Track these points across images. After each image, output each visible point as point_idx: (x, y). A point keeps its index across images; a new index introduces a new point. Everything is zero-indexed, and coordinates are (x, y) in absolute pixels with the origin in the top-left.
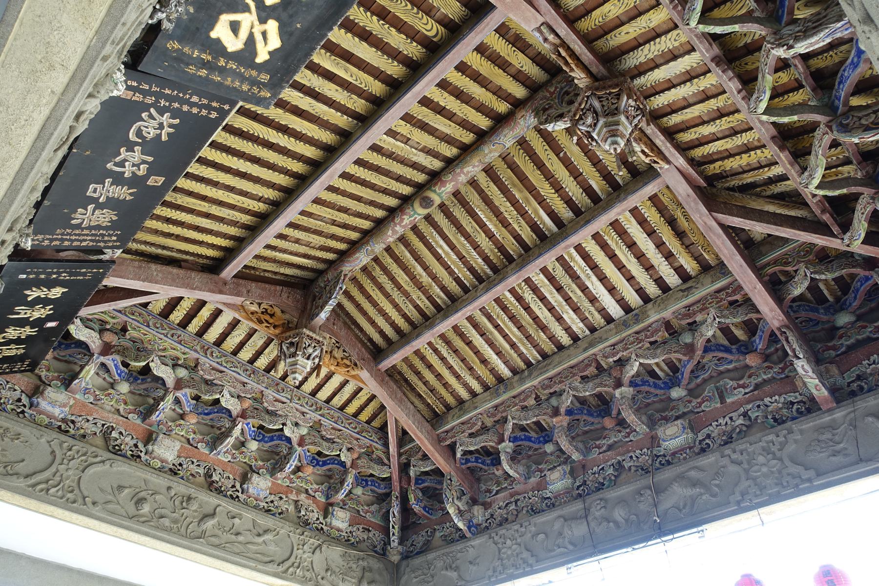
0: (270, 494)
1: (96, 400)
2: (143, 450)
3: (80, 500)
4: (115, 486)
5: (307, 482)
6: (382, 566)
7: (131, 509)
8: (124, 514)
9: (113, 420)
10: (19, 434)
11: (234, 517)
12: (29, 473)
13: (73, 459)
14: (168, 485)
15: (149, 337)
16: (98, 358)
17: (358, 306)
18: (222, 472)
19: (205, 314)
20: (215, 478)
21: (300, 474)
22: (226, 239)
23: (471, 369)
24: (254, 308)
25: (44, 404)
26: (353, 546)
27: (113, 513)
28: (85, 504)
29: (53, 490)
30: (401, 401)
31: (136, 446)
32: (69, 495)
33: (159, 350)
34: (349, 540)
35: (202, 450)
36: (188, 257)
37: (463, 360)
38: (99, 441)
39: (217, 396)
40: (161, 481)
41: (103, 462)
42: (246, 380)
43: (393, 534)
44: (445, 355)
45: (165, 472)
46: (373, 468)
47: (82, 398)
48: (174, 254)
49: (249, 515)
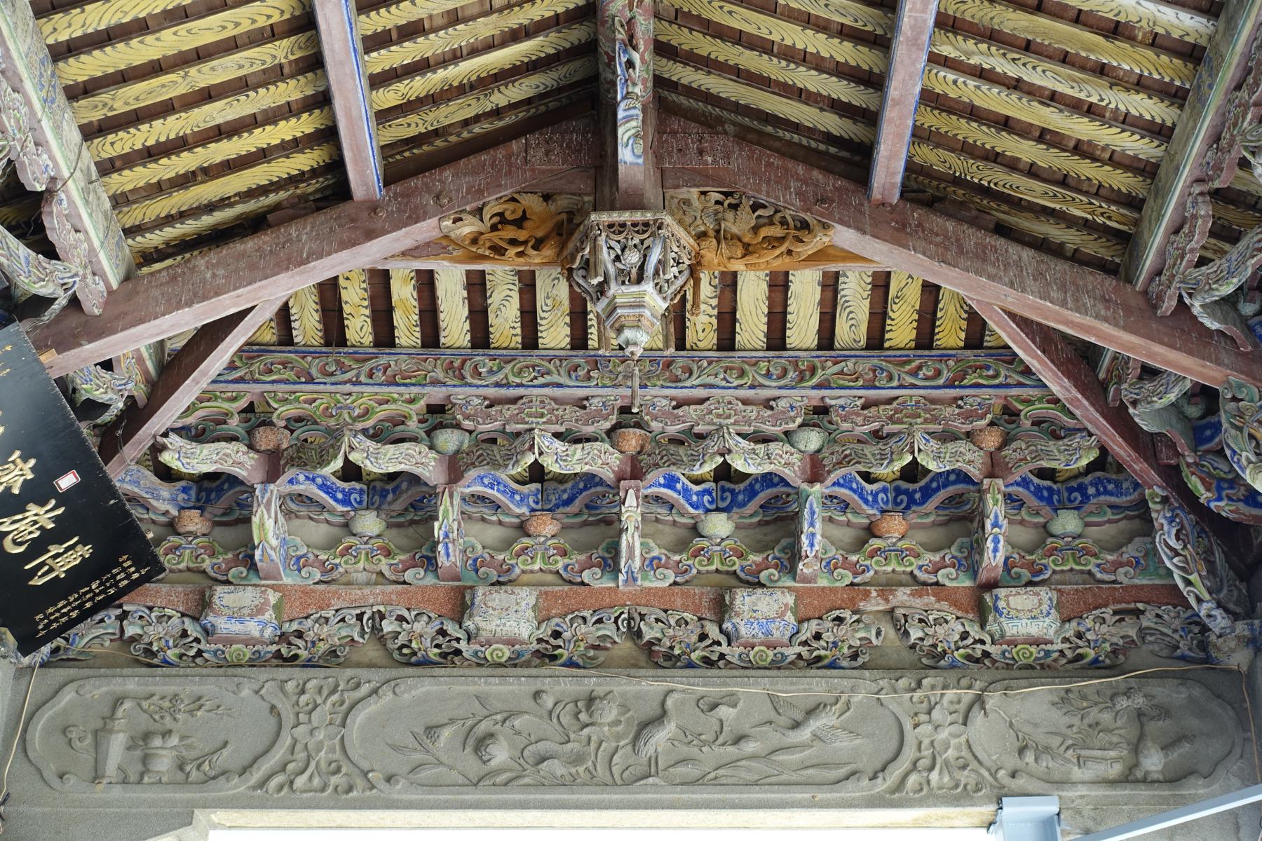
0: (800, 621)
1: (324, 573)
2: (461, 634)
3: (360, 782)
4: (420, 730)
5: (901, 555)
6: (1197, 692)
7: (472, 765)
8: (461, 780)
9: (374, 598)
10: (200, 698)
11: (714, 706)
12: (246, 763)
13: (316, 706)
14: (533, 689)
15: (322, 403)
16: (264, 491)
17: (739, 74)
18: (662, 615)
19: (404, 293)
20: (649, 634)
21: (875, 543)
22: (297, 115)
23: (1101, 70)
24: (468, 227)
25: (223, 625)
26: (1096, 667)
27: (435, 785)
28: (373, 787)
29: (300, 781)
30: (981, 255)
31: (442, 632)
32: (334, 780)
33: (354, 420)
34: (1080, 657)
35: (597, 585)
36: (272, 198)
37: (1064, 59)
38: (371, 652)
39: (530, 459)
40: (515, 687)
41: (375, 691)
42: (581, 393)
43: (1199, 600)
44: (1012, 71)
45: (527, 664)
46: (1048, 453)
47: (299, 581)
48: (240, 209)
49: (753, 690)
